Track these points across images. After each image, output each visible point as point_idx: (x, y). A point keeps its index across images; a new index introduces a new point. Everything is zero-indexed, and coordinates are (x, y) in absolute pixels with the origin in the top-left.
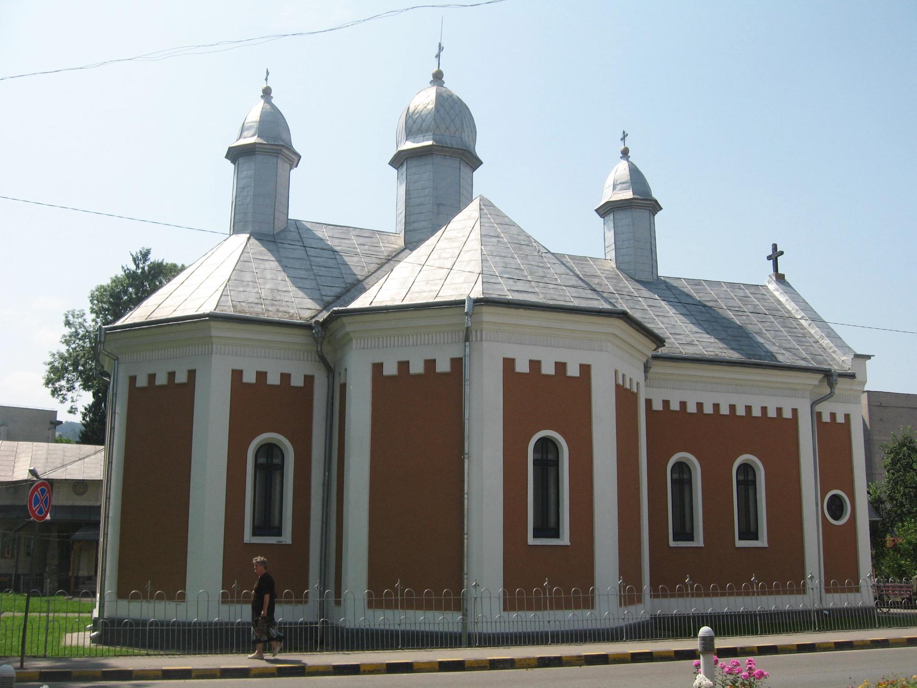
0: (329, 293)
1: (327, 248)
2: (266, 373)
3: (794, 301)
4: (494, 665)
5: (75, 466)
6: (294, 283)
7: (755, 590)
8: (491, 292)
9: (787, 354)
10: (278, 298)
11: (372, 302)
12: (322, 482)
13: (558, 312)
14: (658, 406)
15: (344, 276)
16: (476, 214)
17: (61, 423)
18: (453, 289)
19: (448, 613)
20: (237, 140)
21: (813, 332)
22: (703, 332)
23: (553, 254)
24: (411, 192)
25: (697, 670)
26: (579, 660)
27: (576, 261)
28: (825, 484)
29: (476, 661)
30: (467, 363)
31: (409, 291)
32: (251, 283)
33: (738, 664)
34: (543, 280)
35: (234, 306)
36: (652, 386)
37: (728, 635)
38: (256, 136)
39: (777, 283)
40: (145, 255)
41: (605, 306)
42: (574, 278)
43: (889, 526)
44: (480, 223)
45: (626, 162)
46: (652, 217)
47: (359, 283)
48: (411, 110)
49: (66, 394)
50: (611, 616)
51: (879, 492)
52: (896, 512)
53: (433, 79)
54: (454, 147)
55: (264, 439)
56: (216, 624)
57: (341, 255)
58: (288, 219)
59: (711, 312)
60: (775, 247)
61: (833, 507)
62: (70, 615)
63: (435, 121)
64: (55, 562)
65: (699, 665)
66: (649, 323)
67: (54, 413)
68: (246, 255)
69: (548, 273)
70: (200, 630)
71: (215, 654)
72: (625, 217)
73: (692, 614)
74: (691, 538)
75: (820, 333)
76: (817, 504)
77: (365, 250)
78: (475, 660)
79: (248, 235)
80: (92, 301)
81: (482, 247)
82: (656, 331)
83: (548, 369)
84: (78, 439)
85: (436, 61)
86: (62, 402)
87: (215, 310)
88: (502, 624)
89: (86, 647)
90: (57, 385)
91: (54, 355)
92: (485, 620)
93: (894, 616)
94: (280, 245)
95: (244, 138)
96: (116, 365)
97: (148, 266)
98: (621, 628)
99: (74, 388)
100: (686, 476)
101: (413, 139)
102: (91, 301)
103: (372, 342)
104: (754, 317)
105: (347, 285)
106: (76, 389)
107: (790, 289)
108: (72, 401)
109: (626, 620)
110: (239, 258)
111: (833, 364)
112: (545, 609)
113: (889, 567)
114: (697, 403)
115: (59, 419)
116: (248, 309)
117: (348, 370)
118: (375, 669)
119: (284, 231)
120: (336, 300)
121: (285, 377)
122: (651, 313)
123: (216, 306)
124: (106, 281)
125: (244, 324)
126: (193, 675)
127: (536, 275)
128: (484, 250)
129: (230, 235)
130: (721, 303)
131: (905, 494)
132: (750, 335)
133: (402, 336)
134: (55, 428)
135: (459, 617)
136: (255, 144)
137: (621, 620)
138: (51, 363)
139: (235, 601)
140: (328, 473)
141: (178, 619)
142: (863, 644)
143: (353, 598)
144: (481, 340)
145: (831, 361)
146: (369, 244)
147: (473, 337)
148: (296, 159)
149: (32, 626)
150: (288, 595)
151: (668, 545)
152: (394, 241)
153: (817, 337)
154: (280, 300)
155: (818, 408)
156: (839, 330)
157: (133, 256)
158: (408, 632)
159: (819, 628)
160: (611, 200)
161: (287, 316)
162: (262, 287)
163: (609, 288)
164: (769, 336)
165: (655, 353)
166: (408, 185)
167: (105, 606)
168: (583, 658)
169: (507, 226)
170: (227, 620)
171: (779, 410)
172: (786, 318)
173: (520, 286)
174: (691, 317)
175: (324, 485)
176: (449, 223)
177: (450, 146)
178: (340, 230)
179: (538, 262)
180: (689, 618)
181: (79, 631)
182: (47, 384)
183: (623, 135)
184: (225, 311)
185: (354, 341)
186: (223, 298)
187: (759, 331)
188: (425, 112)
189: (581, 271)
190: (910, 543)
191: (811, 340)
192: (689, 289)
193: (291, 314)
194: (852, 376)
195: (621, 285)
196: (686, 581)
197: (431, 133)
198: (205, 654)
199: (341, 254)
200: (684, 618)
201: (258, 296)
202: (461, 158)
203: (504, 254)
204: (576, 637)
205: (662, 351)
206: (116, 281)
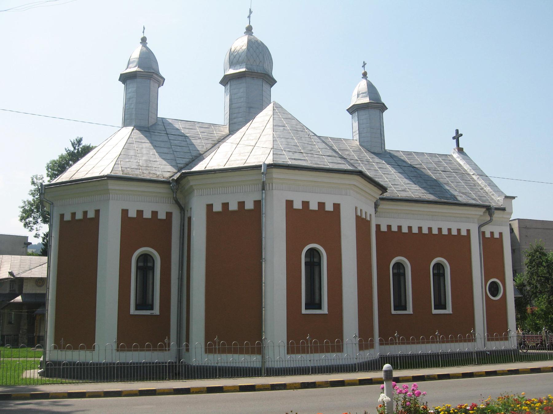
0: (182, 162)
1: (181, 134)
2: (142, 211)
3: (468, 164)
4: (274, 387)
5: (36, 269)
6: (160, 156)
7: (438, 340)
8: (278, 160)
9: (464, 196)
10: (150, 165)
11: (206, 167)
12: (177, 277)
13: (320, 171)
14: (384, 229)
15: (191, 152)
16: (271, 113)
17: (31, 243)
18: (255, 158)
19: (254, 356)
20: (126, 69)
21: (480, 183)
22: (412, 183)
23: (319, 137)
24: (232, 100)
25: (383, 391)
26: (326, 384)
27: (335, 141)
28: (487, 275)
29: (263, 385)
30: (264, 204)
31: (228, 160)
32: (133, 156)
33: (407, 387)
34: (311, 153)
35: (123, 171)
36: (380, 216)
37: (421, 367)
38: (137, 67)
39: (459, 153)
40: (79, 141)
41: (350, 168)
42: (330, 151)
43: (528, 300)
44: (273, 118)
45: (365, 80)
46: (381, 114)
47: (200, 156)
48: (232, 50)
49: (33, 226)
50: (349, 356)
51: (522, 279)
52: (533, 292)
53: (246, 31)
54: (259, 72)
55: (141, 252)
56: (104, 364)
57: (189, 139)
58: (157, 117)
59: (417, 171)
60: (457, 131)
61: (492, 289)
62: (28, 359)
63: (247, 56)
64: (26, 327)
65: (384, 387)
66: (379, 178)
67: (26, 238)
68: (131, 139)
69: (314, 148)
70: (94, 368)
71: (103, 382)
72: (364, 114)
73: (399, 355)
74: (405, 308)
75: (484, 183)
76: (482, 288)
77: (205, 136)
78: (262, 385)
79: (132, 128)
80: (47, 169)
81: (274, 133)
82: (382, 183)
83: (314, 206)
84: (40, 253)
85: (248, 20)
86: (30, 231)
87: (111, 173)
88: (281, 362)
89: (35, 378)
90: (27, 220)
91: (25, 202)
92: (270, 360)
93: (530, 354)
94: (152, 133)
95: (130, 68)
96: (52, 207)
97: (81, 148)
98: (355, 364)
99: (38, 223)
100: (402, 271)
101: (234, 68)
102: (47, 169)
103: (206, 191)
104: (444, 174)
105: (193, 157)
106: (39, 223)
107: (466, 157)
108: (37, 230)
109: (358, 359)
110: (127, 141)
111: (492, 202)
112: (308, 353)
113: (530, 325)
114: (387, 225)
115: (29, 241)
116: (131, 172)
117: (192, 209)
118: (199, 391)
119: (155, 124)
120: (186, 166)
121: (155, 213)
122: (380, 172)
123: (111, 171)
124: (56, 158)
125: (128, 181)
126: (87, 395)
127: (307, 149)
128: (275, 134)
129: (122, 128)
130: (424, 166)
131: (537, 280)
132: (441, 185)
133: (215, 188)
134: (27, 247)
135: (259, 357)
136: (136, 71)
137: (355, 359)
138: (23, 207)
139: (167, 349)
140: (181, 272)
141: (146, 360)
142: (503, 372)
143: (201, 347)
144: (272, 189)
145: (491, 200)
146: (207, 132)
147: (267, 187)
148: (162, 80)
149: (7, 366)
150: (148, 346)
151: (391, 313)
152: (223, 130)
153: (483, 186)
154: (150, 167)
155: (483, 229)
156: (496, 181)
157: (72, 142)
158: (223, 367)
159: (478, 363)
160: (356, 103)
161: (155, 176)
162: (140, 158)
163: (354, 157)
164: (453, 186)
165: (381, 196)
166: (231, 96)
167: (47, 354)
168: (329, 383)
169: (289, 120)
170: (110, 361)
171: (459, 230)
172: (463, 175)
173: (297, 156)
174: (405, 174)
175: (179, 278)
176: (254, 118)
177: (256, 72)
178: (189, 124)
179: (308, 141)
180: (397, 357)
181: (34, 369)
182: (21, 220)
183: (363, 64)
184: (117, 173)
185: (196, 191)
186: (116, 166)
187: (447, 183)
188: (241, 51)
189: (338, 147)
190: (542, 310)
191: (479, 188)
192: (404, 158)
193: (157, 175)
194: (504, 209)
195: (362, 155)
196: (395, 335)
197: (245, 64)
198: (97, 382)
199: (190, 138)
200: (394, 357)
201: (138, 164)
202: (263, 79)
203: (287, 137)
204: (327, 370)
205: (386, 195)
206: (62, 157)
